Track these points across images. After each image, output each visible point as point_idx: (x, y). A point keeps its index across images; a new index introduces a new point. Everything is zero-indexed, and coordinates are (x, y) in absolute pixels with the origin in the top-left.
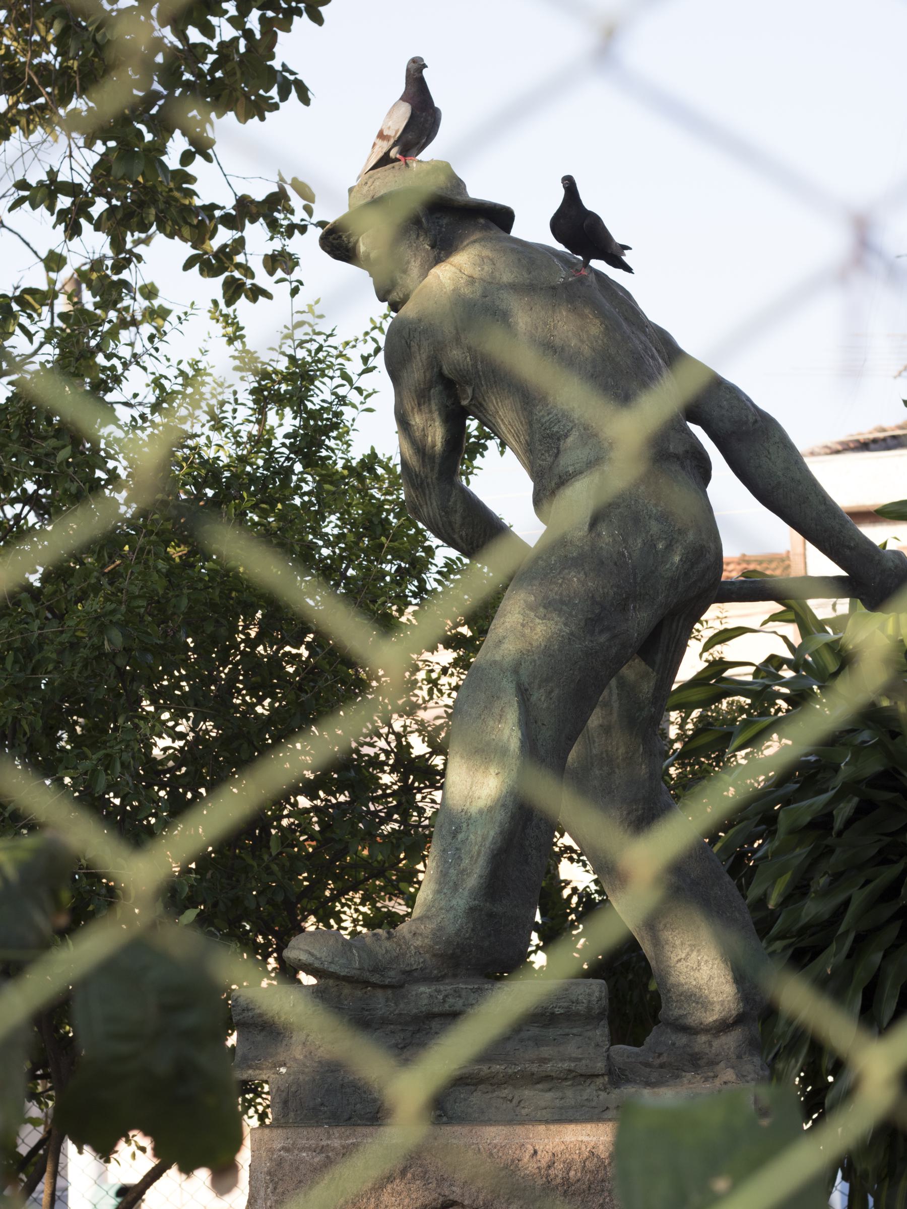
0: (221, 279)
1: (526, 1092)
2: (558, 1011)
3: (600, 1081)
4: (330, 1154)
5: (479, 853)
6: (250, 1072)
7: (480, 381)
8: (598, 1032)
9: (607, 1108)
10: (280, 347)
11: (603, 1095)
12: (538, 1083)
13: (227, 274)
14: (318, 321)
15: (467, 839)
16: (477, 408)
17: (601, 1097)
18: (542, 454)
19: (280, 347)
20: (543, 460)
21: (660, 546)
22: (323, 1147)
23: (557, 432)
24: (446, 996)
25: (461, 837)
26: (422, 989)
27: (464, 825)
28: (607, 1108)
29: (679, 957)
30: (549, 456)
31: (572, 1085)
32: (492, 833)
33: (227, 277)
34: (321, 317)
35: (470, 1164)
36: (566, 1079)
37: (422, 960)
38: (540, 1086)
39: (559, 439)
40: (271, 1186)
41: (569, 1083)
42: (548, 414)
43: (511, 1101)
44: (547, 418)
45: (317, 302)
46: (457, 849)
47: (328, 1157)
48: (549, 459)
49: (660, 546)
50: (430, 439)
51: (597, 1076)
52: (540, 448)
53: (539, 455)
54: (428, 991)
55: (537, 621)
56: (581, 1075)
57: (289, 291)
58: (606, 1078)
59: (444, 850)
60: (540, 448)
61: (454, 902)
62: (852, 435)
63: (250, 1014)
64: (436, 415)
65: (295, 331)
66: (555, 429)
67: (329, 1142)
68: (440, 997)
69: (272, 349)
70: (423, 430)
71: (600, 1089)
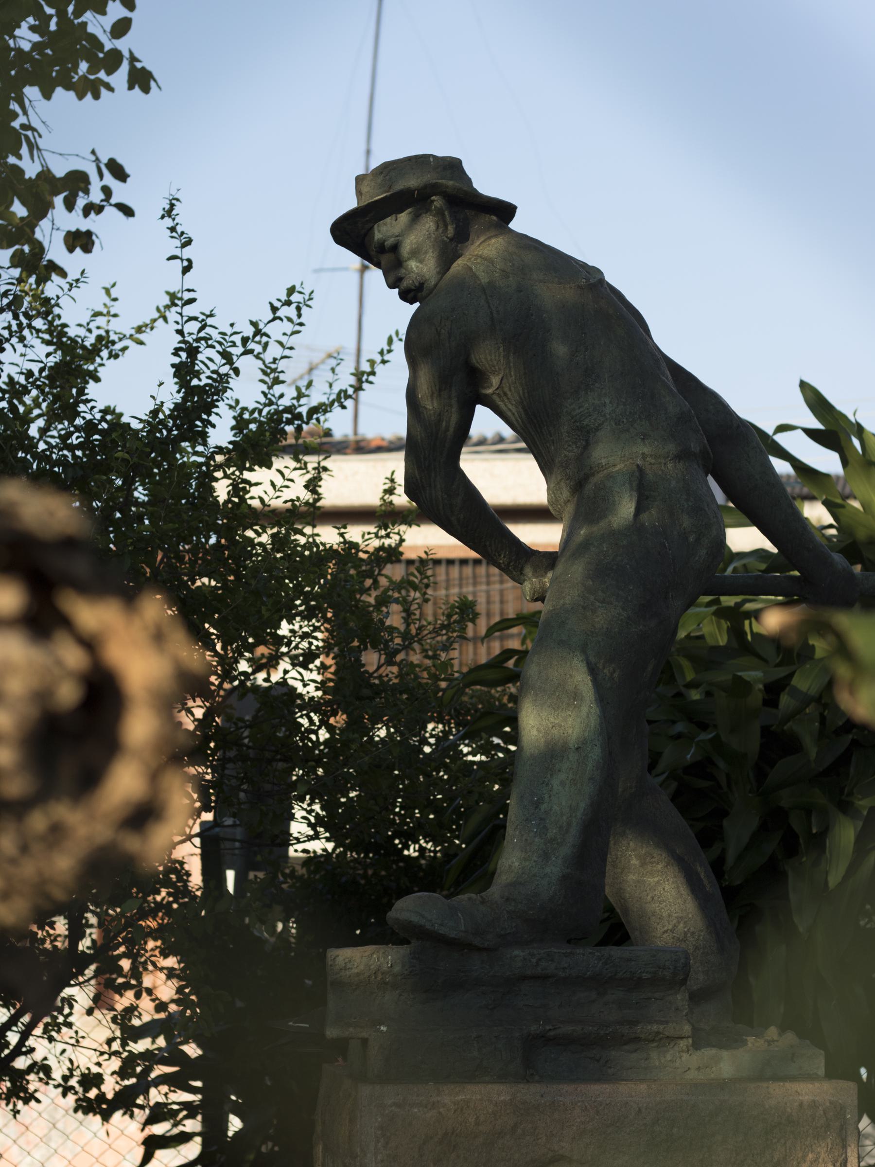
0: (11, 251)
1: (613, 1053)
2: (645, 976)
3: (683, 1044)
4: (441, 1110)
5: (569, 824)
6: (351, 1029)
7: (510, 372)
8: (679, 997)
9: (689, 1069)
10: (88, 324)
11: (685, 1056)
12: (625, 1044)
13: (17, 247)
14: (113, 303)
15: (551, 810)
16: (500, 397)
17: (683, 1059)
18: (569, 446)
19: (88, 324)
20: (569, 451)
21: (691, 539)
22: (434, 1103)
23: (587, 425)
24: (540, 960)
25: (543, 807)
26: (516, 952)
27: (546, 796)
28: (689, 1069)
29: (666, 928)
30: (577, 447)
31: (658, 1047)
32: (583, 805)
33: (17, 250)
34: (115, 300)
35: (578, 1120)
36: (653, 1040)
37: (514, 924)
38: (626, 1047)
39: (588, 432)
40: (382, 1140)
41: (655, 1044)
42: (579, 408)
43: (598, 1061)
44: (577, 411)
45: (114, 285)
46: (541, 819)
47: (440, 1113)
48: (576, 450)
49: (691, 539)
50: (444, 424)
51: (682, 1038)
52: (567, 439)
53: (566, 446)
54: (522, 954)
55: (598, 604)
56: (668, 1037)
57: (181, 269)
58: (690, 1040)
59: (527, 820)
60: (567, 439)
61: (548, 870)
62: (503, 460)
63: (348, 973)
64: (454, 401)
65: (184, 308)
66: (586, 422)
67: (439, 1099)
68: (534, 960)
69: (80, 325)
70: (440, 415)
71: (683, 1051)
